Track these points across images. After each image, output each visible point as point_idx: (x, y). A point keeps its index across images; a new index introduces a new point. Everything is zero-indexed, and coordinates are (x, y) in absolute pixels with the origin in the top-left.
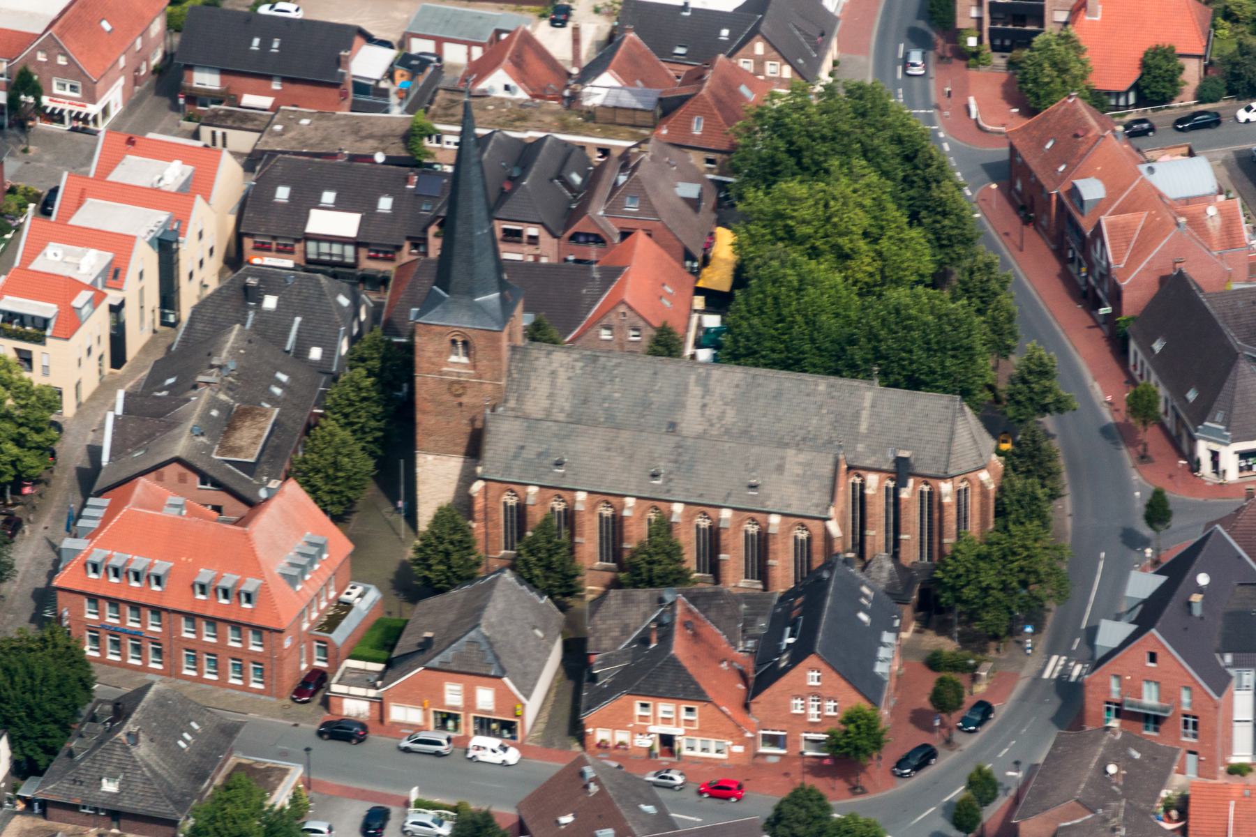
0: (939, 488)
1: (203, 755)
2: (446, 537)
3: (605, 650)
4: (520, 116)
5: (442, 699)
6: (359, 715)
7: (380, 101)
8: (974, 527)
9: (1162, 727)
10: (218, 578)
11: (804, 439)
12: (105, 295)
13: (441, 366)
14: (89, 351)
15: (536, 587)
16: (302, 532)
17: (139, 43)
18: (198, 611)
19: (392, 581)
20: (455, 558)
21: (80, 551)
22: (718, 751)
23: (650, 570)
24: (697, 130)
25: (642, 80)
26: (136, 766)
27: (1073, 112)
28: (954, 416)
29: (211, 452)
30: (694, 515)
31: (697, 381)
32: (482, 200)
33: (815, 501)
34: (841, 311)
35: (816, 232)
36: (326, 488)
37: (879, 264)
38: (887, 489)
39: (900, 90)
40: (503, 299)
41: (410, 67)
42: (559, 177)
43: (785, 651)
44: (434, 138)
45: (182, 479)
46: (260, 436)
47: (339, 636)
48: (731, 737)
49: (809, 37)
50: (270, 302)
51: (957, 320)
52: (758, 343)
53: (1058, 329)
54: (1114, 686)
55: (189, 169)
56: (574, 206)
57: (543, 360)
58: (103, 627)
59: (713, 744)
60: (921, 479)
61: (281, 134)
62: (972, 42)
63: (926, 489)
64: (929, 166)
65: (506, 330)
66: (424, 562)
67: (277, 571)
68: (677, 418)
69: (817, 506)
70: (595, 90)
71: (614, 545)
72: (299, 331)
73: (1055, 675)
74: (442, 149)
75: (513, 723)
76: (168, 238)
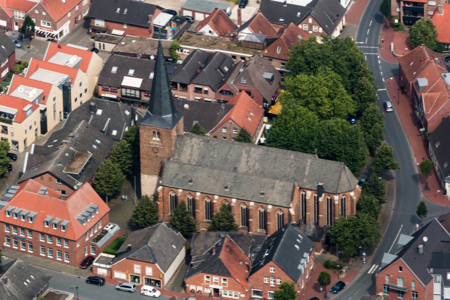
0: (334, 198)
1: (33, 288)
2: (144, 207)
3: (198, 255)
4: (213, 43)
5: (133, 271)
6: (103, 275)
7: (164, 34)
8: (348, 212)
9: (405, 296)
10: (53, 219)
11: (284, 176)
12: (38, 106)
13: (149, 141)
14: (31, 127)
15: (177, 228)
16: (89, 203)
17: (77, 8)
18: (45, 232)
20: (148, 216)
21: (4, 206)
22: (235, 296)
23: (219, 224)
24: (278, 51)
25: (262, 31)
26: (5, 292)
27: (421, 51)
28: (341, 171)
29: (63, 170)
30: (240, 204)
31: (246, 151)
32: (165, 78)
33: (285, 201)
34: (310, 126)
35: (309, 95)
36: (106, 186)
38: (315, 197)
40: (173, 117)
41: (177, 22)
44: (180, 50)
45: (50, 180)
46: (83, 164)
47: (100, 244)
48: (240, 291)
49: (331, 17)
50: (99, 112)
51: (351, 133)
52: (278, 137)
53: (406, 136)
54: (387, 279)
55: (80, 58)
56: (223, 80)
58: (11, 236)
59: (233, 293)
60: (327, 194)
61: (124, 46)
62: (396, 21)
64: (360, 70)
66: (136, 216)
67: (76, 218)
68: (237, 166)
69: (286, 202)
70: (242, 34)
72: (109, 124)
73: (373, 272)
74: (183, 54)
75: (160, 281)
76: (67, 85)
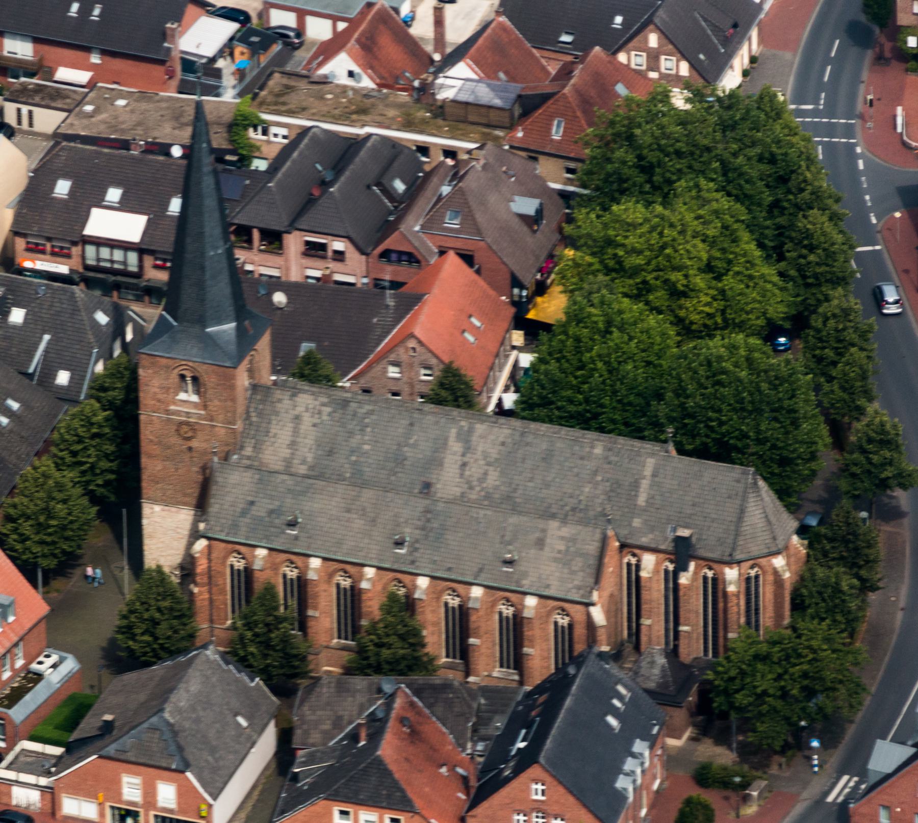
0: (723, 574)
2: (153, 602)
3: (313, 745)
5: (119, 794)
6: (29, 806)
7: (212, 82)
8: (767, 618)
11: (574, 509)
13: (168, 404)
19: (103, 649)
20: (163, 629)
23: (378, 654)
24: (557, 134)
25: (506, 73)
28: (745, 492)
31: (459, 437)
33: (576, 582)
34: (652, 358)
35: (648, 263)
36: (37, 538)
37: (721, 304)
38: (666, 572)
39: (823, 95)
41: (250, 44)
42: (378, 184)
43: (514, 756)
44: (260, 129)
49: (716, 29)
51: (777, 378)
52: (554, 392)
57: (287, 402)
61: (90, 116)
63: (710, 574)
64: (802, 190)
65: (245, 364)
66: (127, 630)
68: (433, 478)
69: (579, 588)
71: (353, 620)
72: (46, 351)
74: (269, 142)
